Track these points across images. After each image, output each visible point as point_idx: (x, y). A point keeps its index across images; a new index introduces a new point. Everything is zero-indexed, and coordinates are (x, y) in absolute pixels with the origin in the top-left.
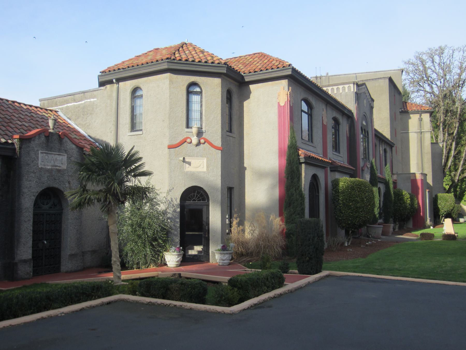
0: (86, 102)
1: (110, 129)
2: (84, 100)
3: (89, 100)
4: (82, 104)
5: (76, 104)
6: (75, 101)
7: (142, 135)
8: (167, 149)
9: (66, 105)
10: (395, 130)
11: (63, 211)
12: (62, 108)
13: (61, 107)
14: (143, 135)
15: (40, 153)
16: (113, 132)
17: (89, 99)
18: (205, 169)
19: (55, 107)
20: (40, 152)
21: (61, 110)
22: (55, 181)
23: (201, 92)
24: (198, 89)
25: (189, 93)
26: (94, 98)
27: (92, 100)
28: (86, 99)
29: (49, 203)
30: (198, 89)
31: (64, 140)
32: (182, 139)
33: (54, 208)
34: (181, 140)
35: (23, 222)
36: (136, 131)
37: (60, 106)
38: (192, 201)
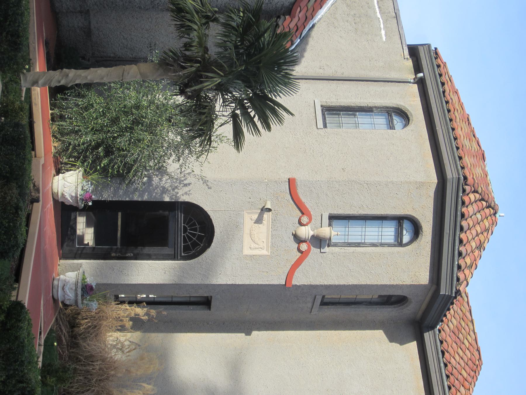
3: (382, 26)
16: (321, 71)
17: (385, 27)
18: (247, 251)
23: (399, 243)
24: (406, 238)
26: (386, 35)
27: (383, 32)
30: (406, 238)
36: (323, 115)
38: (184, 226)
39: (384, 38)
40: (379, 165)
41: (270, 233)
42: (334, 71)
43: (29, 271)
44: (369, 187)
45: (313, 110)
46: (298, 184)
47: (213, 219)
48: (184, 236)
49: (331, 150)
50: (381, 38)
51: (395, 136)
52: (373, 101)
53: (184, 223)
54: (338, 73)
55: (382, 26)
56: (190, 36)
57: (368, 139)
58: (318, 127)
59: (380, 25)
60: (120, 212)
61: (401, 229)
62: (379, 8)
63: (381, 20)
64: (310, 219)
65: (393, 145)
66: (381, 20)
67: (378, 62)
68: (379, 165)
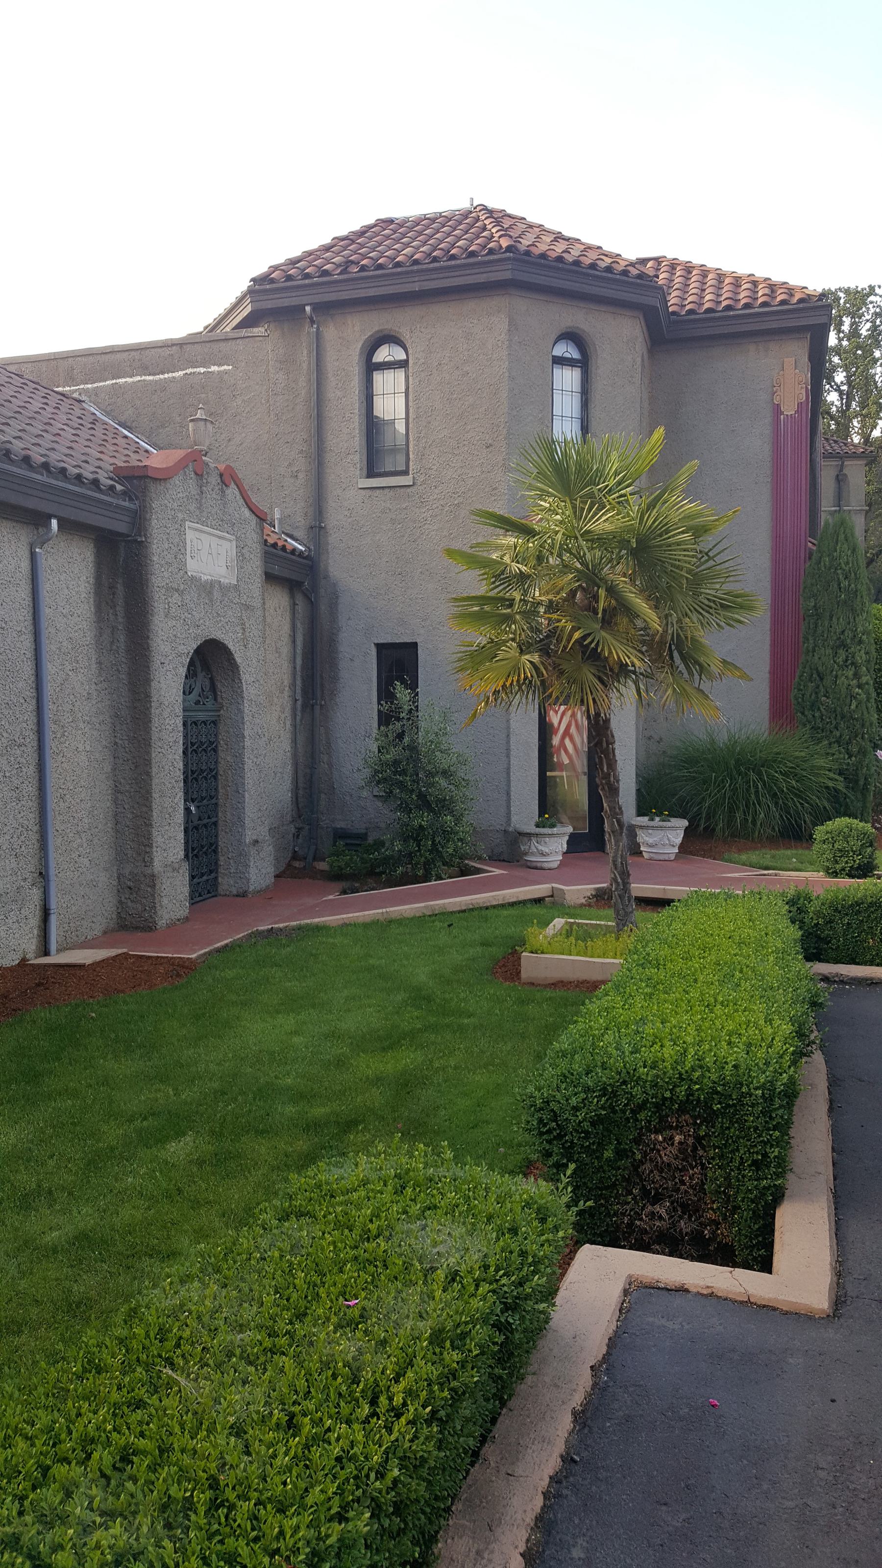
1: (290, 465)
3: (202, 370)
7: (409, 490)
26: (220, 365)
39: (226, 367)
50: (226, 372)
52: (357, 392)
55: (202, 370)
63: (189, 371)
66: (189, 371)
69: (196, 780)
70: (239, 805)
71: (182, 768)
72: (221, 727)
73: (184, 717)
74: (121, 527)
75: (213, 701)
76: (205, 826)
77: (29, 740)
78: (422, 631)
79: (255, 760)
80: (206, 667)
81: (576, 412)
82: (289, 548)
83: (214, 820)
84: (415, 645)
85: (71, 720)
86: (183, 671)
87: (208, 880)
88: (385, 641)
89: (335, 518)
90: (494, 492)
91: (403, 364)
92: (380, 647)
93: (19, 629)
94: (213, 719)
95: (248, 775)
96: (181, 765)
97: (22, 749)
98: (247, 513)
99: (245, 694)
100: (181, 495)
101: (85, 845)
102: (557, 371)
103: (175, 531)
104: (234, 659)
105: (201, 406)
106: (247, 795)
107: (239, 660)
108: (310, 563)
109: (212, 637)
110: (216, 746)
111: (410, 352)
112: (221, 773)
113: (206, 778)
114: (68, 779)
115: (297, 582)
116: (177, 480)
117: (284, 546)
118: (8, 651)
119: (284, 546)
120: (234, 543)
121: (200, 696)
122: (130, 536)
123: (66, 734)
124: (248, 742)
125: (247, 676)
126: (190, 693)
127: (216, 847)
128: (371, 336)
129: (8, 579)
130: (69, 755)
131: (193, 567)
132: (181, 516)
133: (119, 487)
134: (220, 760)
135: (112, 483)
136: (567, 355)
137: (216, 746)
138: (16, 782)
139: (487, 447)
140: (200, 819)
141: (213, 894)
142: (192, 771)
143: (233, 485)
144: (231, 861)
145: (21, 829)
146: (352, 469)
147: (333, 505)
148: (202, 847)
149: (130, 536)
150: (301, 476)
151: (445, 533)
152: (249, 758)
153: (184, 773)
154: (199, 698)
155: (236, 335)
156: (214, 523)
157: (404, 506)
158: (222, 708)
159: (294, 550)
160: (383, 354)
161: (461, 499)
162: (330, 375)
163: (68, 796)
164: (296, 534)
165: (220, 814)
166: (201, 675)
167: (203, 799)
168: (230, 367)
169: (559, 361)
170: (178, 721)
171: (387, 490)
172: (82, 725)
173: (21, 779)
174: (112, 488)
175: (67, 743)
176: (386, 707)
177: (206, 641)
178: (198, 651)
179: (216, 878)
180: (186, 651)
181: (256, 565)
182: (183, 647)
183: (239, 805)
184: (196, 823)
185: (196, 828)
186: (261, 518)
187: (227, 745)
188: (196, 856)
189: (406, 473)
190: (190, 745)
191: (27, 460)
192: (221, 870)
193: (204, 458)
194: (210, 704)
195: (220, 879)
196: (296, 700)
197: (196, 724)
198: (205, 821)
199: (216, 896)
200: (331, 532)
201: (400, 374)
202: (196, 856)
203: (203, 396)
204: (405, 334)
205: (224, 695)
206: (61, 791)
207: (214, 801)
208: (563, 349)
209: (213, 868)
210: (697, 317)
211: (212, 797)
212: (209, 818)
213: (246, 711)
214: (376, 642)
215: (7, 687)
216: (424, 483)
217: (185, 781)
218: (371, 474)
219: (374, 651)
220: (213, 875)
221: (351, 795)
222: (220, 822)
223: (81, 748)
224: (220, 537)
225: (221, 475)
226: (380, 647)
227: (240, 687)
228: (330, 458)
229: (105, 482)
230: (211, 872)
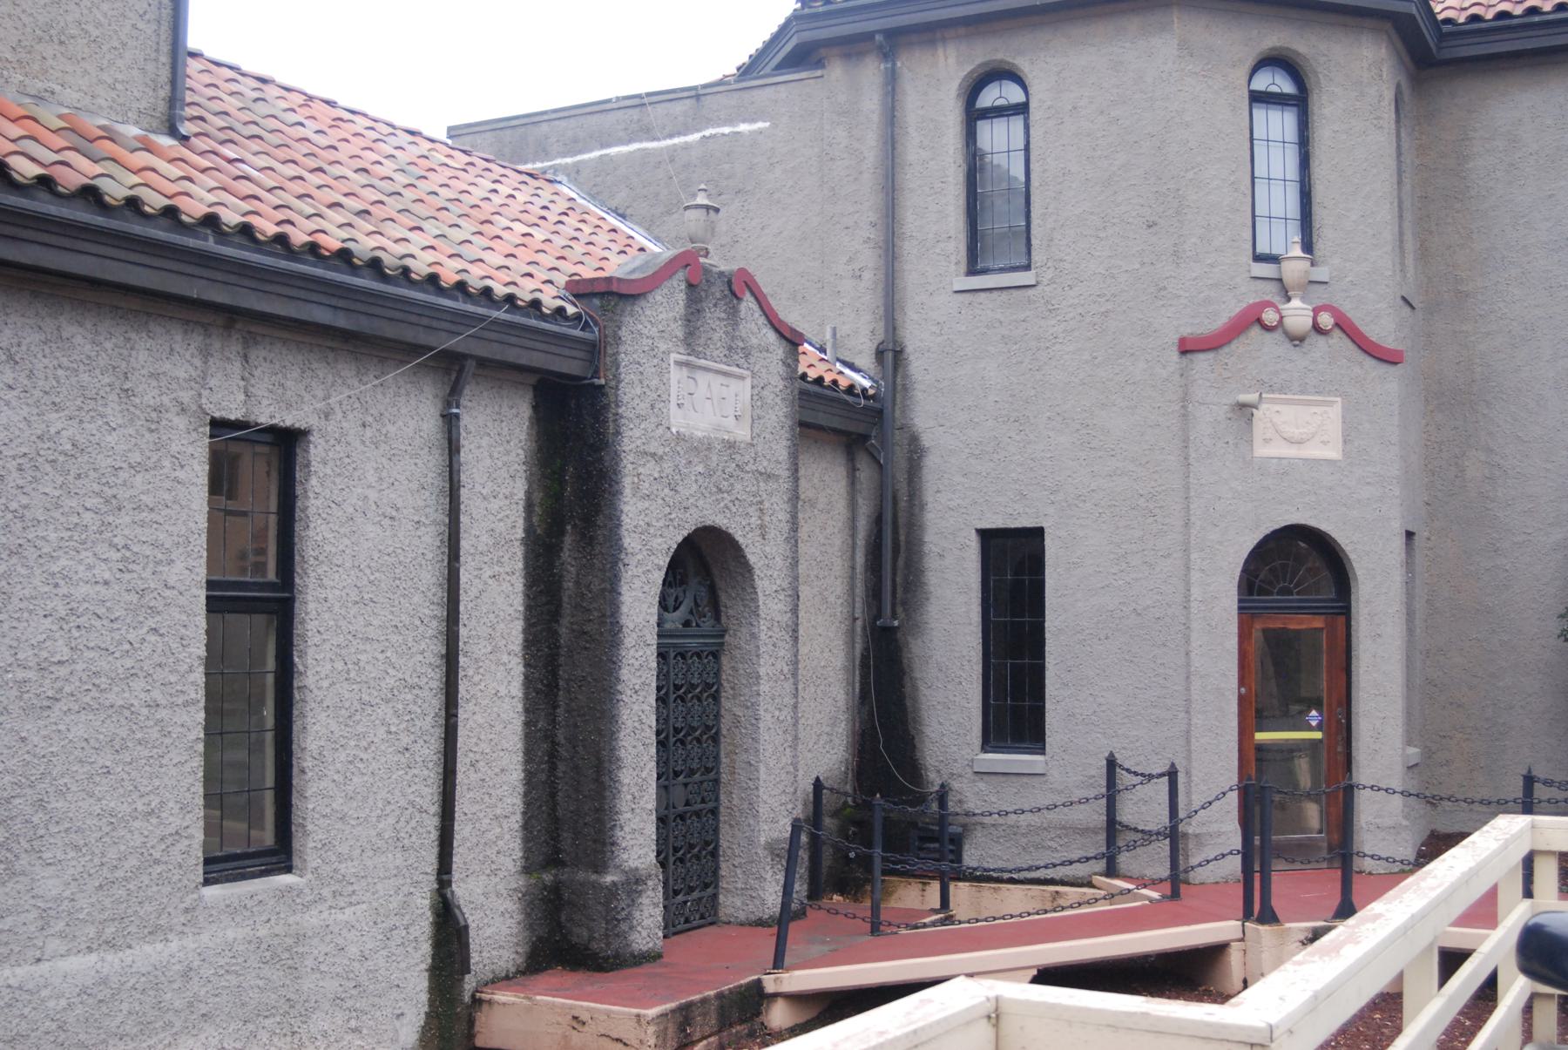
0: (712, 136)
1: (850, 260)
2: (698, 130)
3: (726, 130)
4: (687, 147)
5: (654, 145)
6: (647, 132)
7: (1030, 292)
8: (1174, 355)
9: (596, 154)
10: (1412, 307)
11: (727, 637)
12: (576, 164)
13: (569, 160)
14: (1039, 288)
15: (672, 363)
16: (868, 275)
17: (730, 121)
18: (1333, 453)
19: (534, 162)
20: (674, 357)
21: (568, 175)
22: (719, 497)
23: (1022, 109)
24: (1013, 94)
25: (973, 116)
26: (753, 121)
27: (744, 127)
28: (710, 122)
29: (681, 603)
30: (1013, 94)
31: (743, 306)
32: (1238, 310)
33: (698, 625)
34: (1233, 314)
35: (629, 693)
36: (984, 271)
37: (564, 155)
38: (1278, 594)
39: (760, 125)
40: (1136, 142)
41: (1296, 397)
42: (867, 245)
43: (1462, 933)
44: (1193, 168)
45: (983, 295)
46: (1190, 331)
47: (1271, 529)
48: (1298, 593)
49: (1098, 254)
50: (760, 132)
51: (1049, 103)
52: (951, 152)
53: (1269, 593)
54: (872, 236)
55: (726, 130)
56: (266, 577)
57: (1062, 166)
58: (1033, 283)
59: (723, 135)
60: (1253, 736)
61: (1289, 100)
62: (671, 136)
63: (707, 133)
64: (1269, 304)
65: (1075, 108)
66: (707, 133)
67: (834, 141)
68: (1136, 142)
69: (682, 742)
70: (751, 783)
71: (654, 724)
72: (725, 660)
73: (659, 646)
74: (570, 366)
75: (712, 622)
76: (698, 814)
77: (426, 680)
78: (1051, 510)
79: (777, 713)
80: (705, 571)
81: (1292, 172)
82: (843, 383)
83: (711, 805)
84: (1038, 533)
85: (489, 649)
86: (659, 577)
87: (700, 899)
88: (994, 526)
89: (917, 338)
90: (1163, 293)
91: (1022, 109)
92: (986, 536)
93: (416, 519)
94: (714, 648)
95: (764, 736)
96: (652, 720)
97: (415, 692)
98: (771, 336)
99: (763, 612)
100: (663, 316)
101: (507, 837)
102: (1260, 113)
103: (653, 370)
104: (745, 557)
105: (703, 186)
106: (762, 769)
107: (752, 559)
108: (878, 405)
109: (709, 523)
110: (717, 691)
111: (1031, 91)
112: (724, 732)
113: (698, 740)
114: (482, 737)
115: (860, 435)
116: (658, 296)
117: (835, 382)
118: (400, 551)
119: (835, 382)
120: (748, 382)
121: (691, 612)
122: (585, 378)
123: (481, 670)
124: (764, 687)
125: (766, 583)
126: (676, 609)
127: (716, 848)
128: (972, 72)
129: (403, 448)
130: (484, 703)
131: (678, 421)
132: (663, 346)
133: (571, 310)
134: (723, 712)
135: (560, 303)
136: (1274, 89)
137: (717, 691)
138: (406, 740)
139: (1150, 227)
140: (687, 804)
141: (710, 920)
142: (675, 729)
143: (748, 297)
144: (739, 871)
145: (411, 810)
146: (944, 264)
147: (915, 317)
148: (692, 846)
149: (585, 378)
150: (867, 275)
151: (1086, 356)
152: (766, 710)
153: (658, 733)
154: (690, 617)
155: (744, 84)
156: (716, 353)
157: (1022, 316)
158: (725, 631)
159: (851, 389)
160: (990, 97)
161: (1109, 306)
162: (910, 130)
163: (482, 763)
164: (858, 362)
165: (722, 797)
166: (693, 582)
167: (692, 772)
168: (767, 124)
169: (1257, 98)
170: (649, 652)
171: (995, 294)
172: (505, 658)
173: (412, 737)
174: (560, 311)
175: (483, 684)
176: (445, 877)
177: (697, 530)
178: (688, 541)
179: (715, 896)
180: (666, 546)
181: (778, 415)
182: (660, 540)
183: (751, 783)
184: (681, 808)
185: (682, 817)
186: (792, 340)
187: (733, 688)
188: (681, 860)
189: (1027, 267)
190: (672, 688)
191: (433, 279)
192: (723, 884)
193: (702, 260)
194: (707, 624)
195: (721, 898)
196: (855, 619)
197: (683, 657)
198: (698, 807)
199: (712, 924)
200: (911, 358)
201: (1017, 123)
202: (681, 860)
203: (727, 166)
204: (1023, 64)
205: (731, 612)
206: (471, 755)
207: (712, 775)
208: (1267, 81)
209: (710, 881)
210: (1483, 25)
211: (708, 770)
212: (703, 801)
213: (763, 636)
214: (979, 527)
215: (397, 602)
216: (1052, 281)
217: (661, 744)
218: (972, 271)
219: (974, 545)
220: (710, 891)
221: (939, 771)
222: (722, 809)
223: (503, 692)
224: (725, 374)
225: (729, 283)
226: (986, 536)
227: (755, 600)
228: (909, 250)
229: (549, 301)
230: (706, 886)
